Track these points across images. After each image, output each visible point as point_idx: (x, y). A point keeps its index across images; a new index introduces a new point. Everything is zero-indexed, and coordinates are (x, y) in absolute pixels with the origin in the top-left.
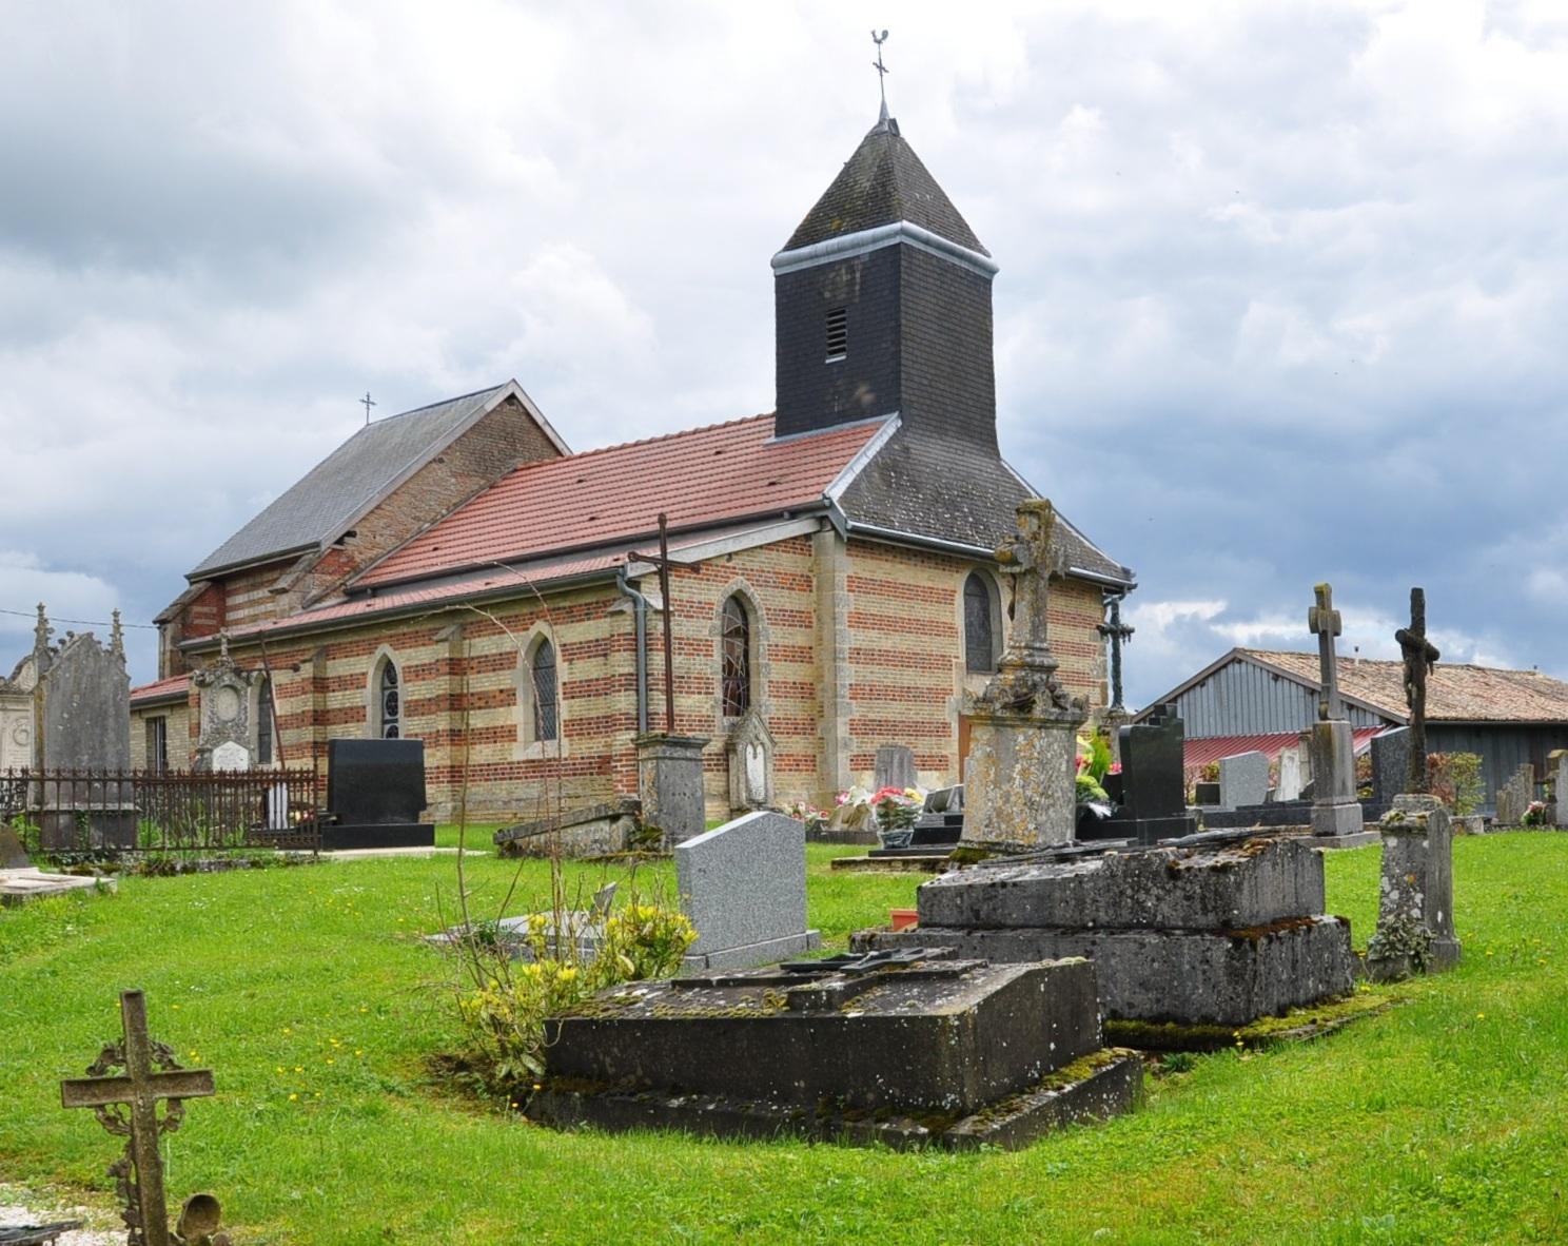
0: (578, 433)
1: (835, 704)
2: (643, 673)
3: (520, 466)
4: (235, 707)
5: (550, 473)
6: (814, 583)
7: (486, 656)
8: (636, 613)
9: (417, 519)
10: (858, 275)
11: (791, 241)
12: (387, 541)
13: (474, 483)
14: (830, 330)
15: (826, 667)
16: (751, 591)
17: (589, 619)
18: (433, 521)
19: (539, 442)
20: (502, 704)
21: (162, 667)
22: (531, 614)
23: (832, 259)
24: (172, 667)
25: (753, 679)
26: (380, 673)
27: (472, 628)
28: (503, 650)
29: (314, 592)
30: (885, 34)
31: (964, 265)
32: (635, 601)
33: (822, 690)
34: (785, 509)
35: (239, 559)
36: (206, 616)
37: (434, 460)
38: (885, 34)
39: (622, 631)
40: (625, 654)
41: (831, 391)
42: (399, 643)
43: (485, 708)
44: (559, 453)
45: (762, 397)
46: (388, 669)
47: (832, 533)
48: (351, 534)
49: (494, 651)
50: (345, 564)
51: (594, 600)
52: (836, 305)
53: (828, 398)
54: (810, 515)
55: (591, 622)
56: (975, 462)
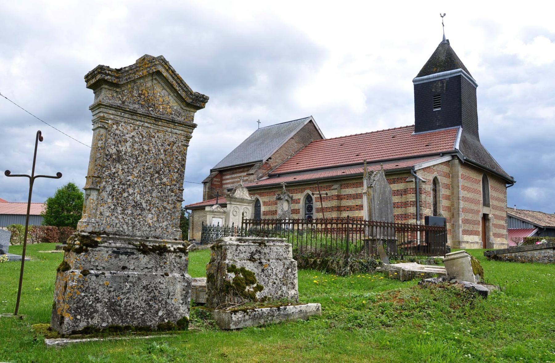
0: (327, 134)
1: (459, 213)
2: (418, 201)
3: (313, 141)
4: (287, 207)
5: (322, 143)
6: (451, 176)
7: (351, 195)
8: (416, 182)
9: (287, 155)
10: (445, 84)
11: (419, 74)
12: (279, 161)
13: (301, 145)
14: (434, 101)
15: (455, 202)
16: (438, 177)
17: (394, 183)
18: (291, 156)
19: (317, 135)
20: (357, 210)
21: (204, 196)
22: (398, 178)
23: (435, 80)
24: (208, 196)
25: (437, 205)
26: (305, 199)
27: (344, 185)
28: (358, 193)
29: (260, 175)
30: (445, 15)
31: (472, 83)
32: (416, 178)
33: (454, 209)
34: (441, 153)
35: (231, 165)
36: (217, 181)
37: (291, 138)
38: (445, 15)
39: (411, 187)
40: (413, 195)
41: (435, 119)
42: (261, 195)
43: (350, 211)
44: (322, 138)
45: (410, 120)
46: (309, 199)
47: (458, 160)
48: (270, 158)
49: (354, 193)
50: (268, 167)
51: (397, 177)
52: (437, 93)
53: (435, 121)
54: (449, 155)
55: (396, 184)
56: (476, 142)
